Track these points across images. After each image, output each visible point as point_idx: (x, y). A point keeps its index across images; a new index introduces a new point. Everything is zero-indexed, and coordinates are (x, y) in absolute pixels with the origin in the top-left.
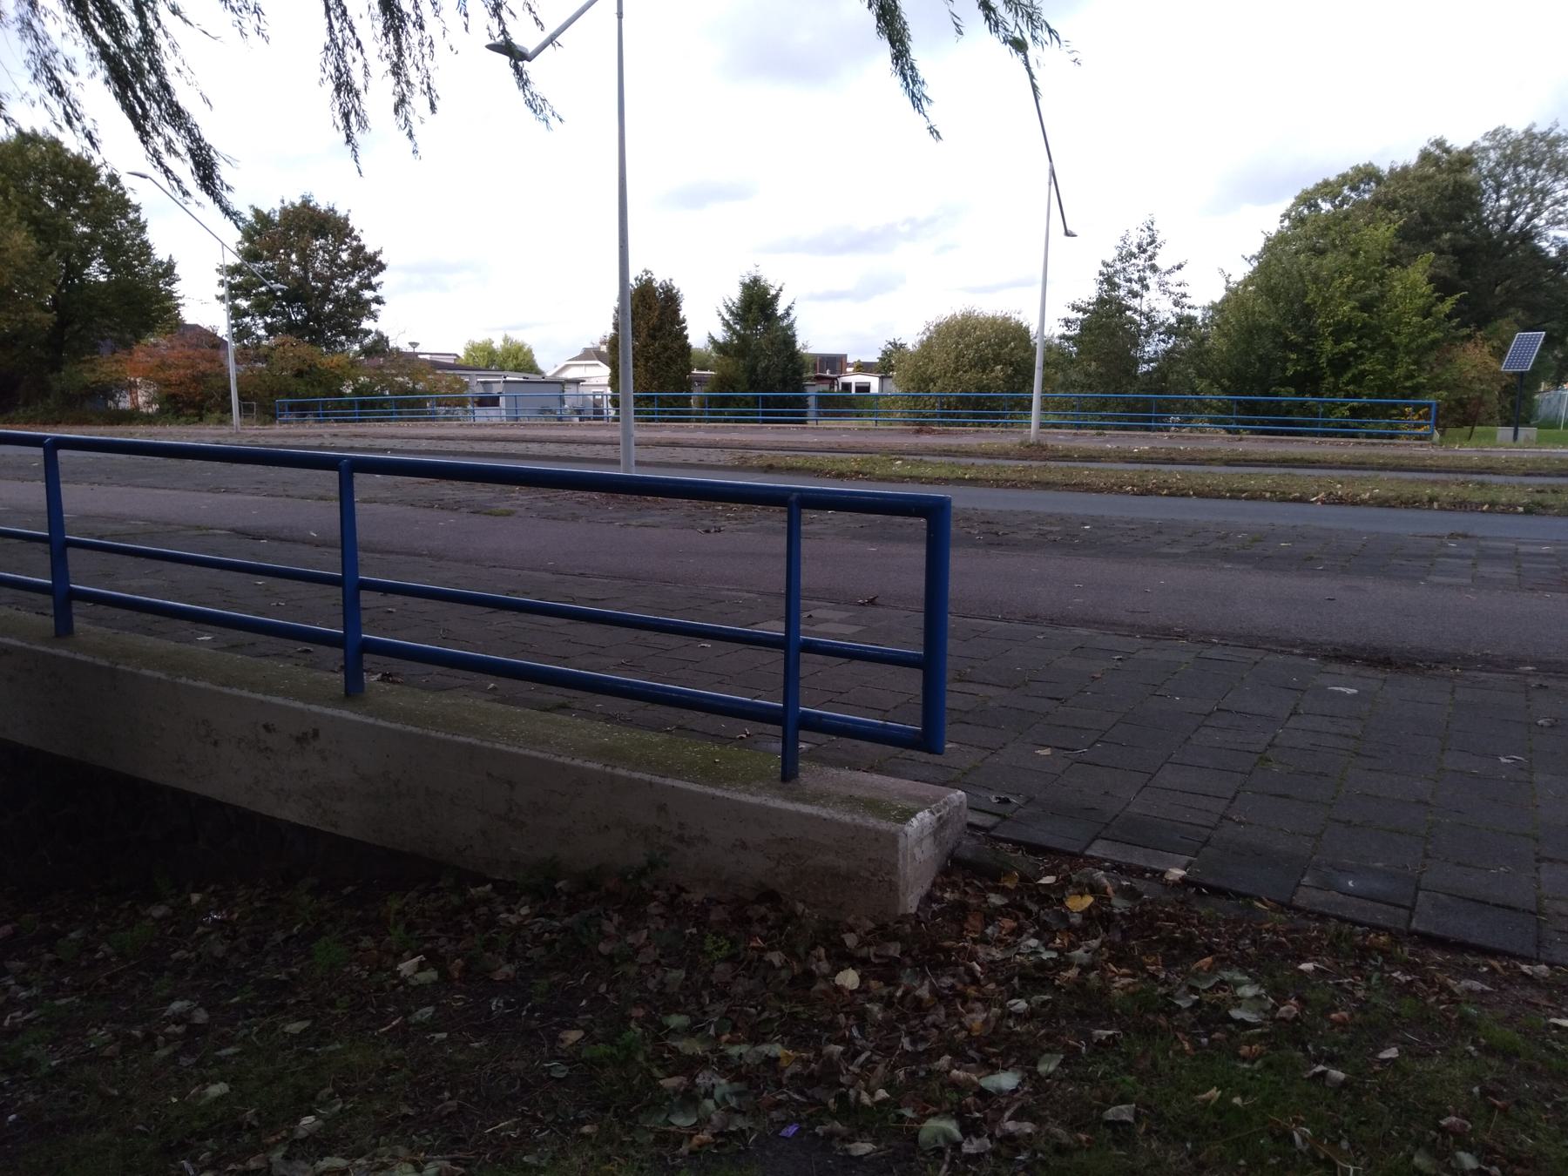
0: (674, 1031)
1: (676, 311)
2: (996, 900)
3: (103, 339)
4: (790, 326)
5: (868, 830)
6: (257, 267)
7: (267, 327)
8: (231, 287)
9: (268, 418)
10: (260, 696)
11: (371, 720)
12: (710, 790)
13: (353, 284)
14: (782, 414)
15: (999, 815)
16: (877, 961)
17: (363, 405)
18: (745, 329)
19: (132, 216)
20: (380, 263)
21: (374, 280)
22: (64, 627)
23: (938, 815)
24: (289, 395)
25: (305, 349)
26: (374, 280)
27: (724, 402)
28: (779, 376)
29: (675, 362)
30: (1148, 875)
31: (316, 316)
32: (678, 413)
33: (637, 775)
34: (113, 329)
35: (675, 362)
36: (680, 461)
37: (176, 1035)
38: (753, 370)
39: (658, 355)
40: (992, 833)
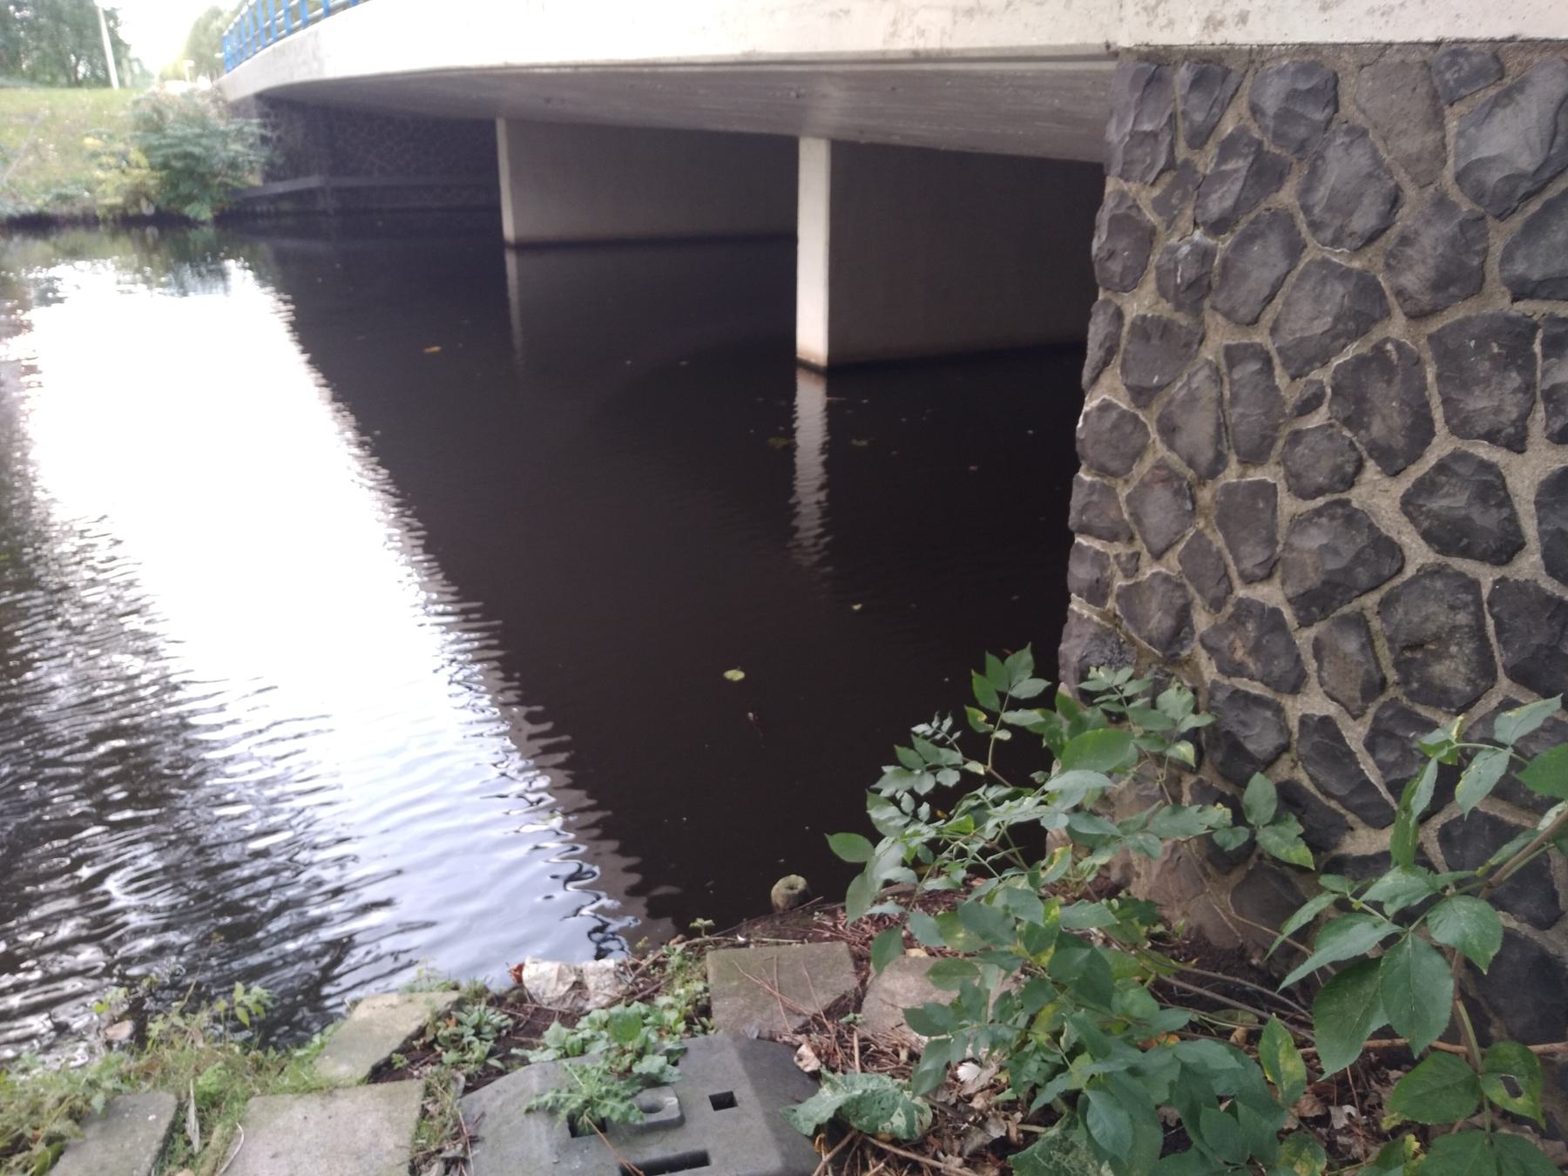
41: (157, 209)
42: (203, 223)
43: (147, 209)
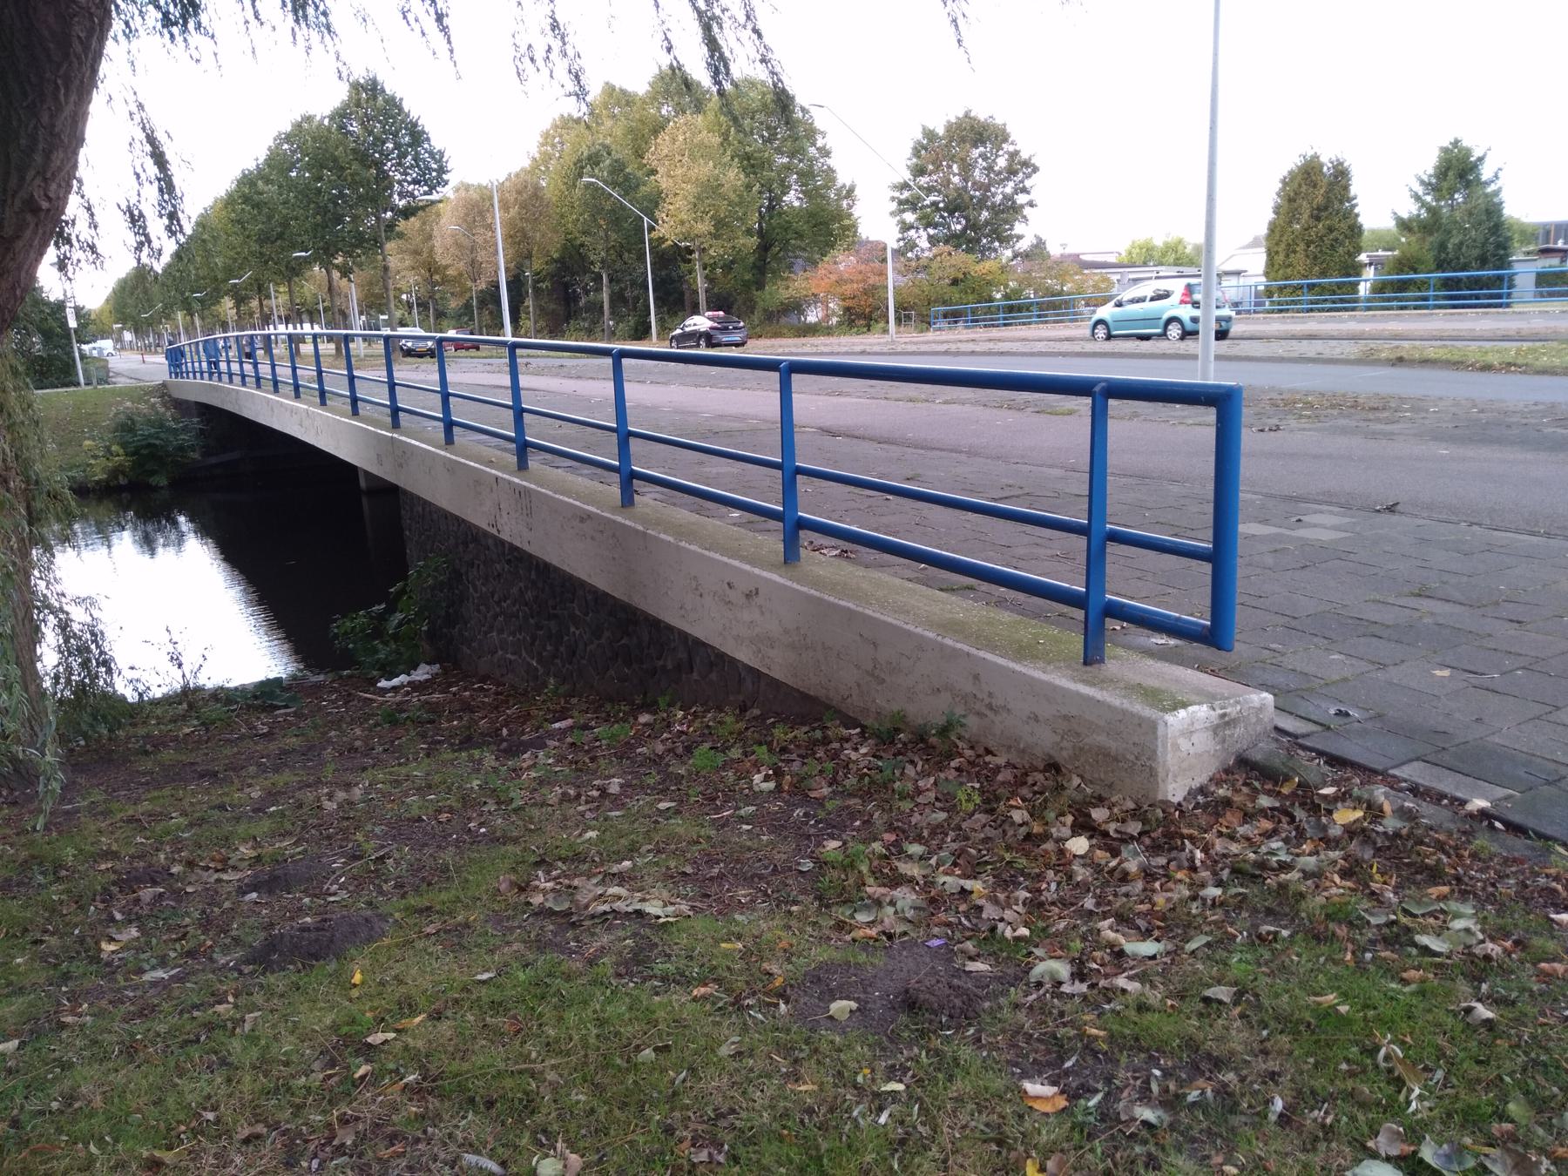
0: (910, 857)
1: (1346, 188)
2: (1265, 801)
3: (796, 257)
4: (1497, 193)
5: (1133, 715)
6: (923, 180)
7: (930, 238)
8: (901, 203)
9: (925, 326)
10: (725, 559)
11: (789, 583)
12: (1012, 665)
13: (1009, 190)
14: (1477, 297)
15: (1321, 725)
16: (1115, 836)
17: (1011, 309)
18: (1437, 200)
19: (820, 143)
20: (1033, 165)
21: (1028, 183)
22: (628, 499)
23: (1220, 712)
24: (945, 303)
25: (960, 259)
26: (1028, 183)
27: (1402, 286)
28: (1476, 252)
29: (1342, 244)
30: (1445, 801)
31: (972, 225)
32: (1342, 301)
33: (959, 646)
34: (805, 250)
35: (1342, 244)
36: (1296, 355)
37: (593, 797)
38: (1442, 247)
39: (1321, 238)
40: (1300, 741)
41: (130, 482)
42: (162, 488)
43: (122, 481)
